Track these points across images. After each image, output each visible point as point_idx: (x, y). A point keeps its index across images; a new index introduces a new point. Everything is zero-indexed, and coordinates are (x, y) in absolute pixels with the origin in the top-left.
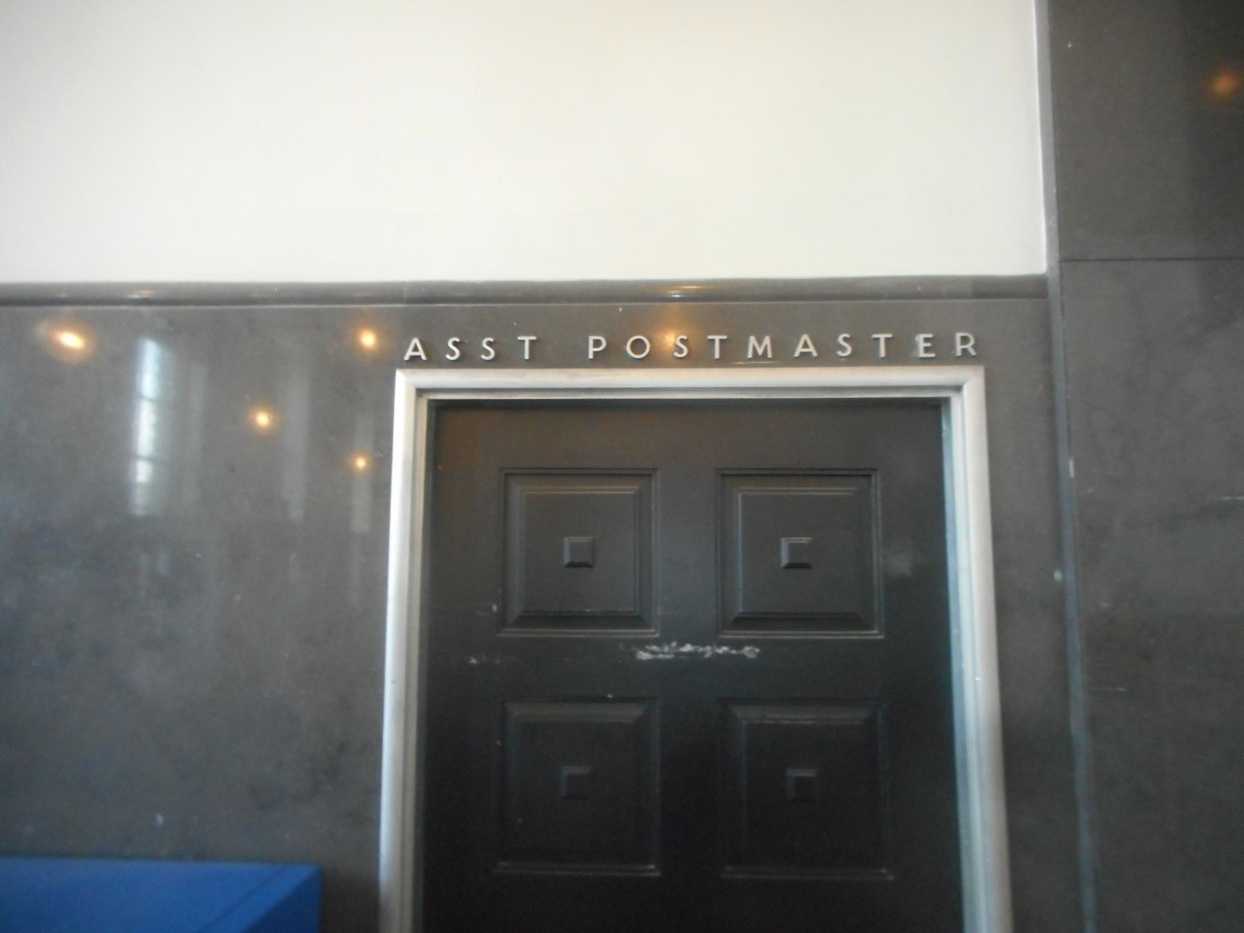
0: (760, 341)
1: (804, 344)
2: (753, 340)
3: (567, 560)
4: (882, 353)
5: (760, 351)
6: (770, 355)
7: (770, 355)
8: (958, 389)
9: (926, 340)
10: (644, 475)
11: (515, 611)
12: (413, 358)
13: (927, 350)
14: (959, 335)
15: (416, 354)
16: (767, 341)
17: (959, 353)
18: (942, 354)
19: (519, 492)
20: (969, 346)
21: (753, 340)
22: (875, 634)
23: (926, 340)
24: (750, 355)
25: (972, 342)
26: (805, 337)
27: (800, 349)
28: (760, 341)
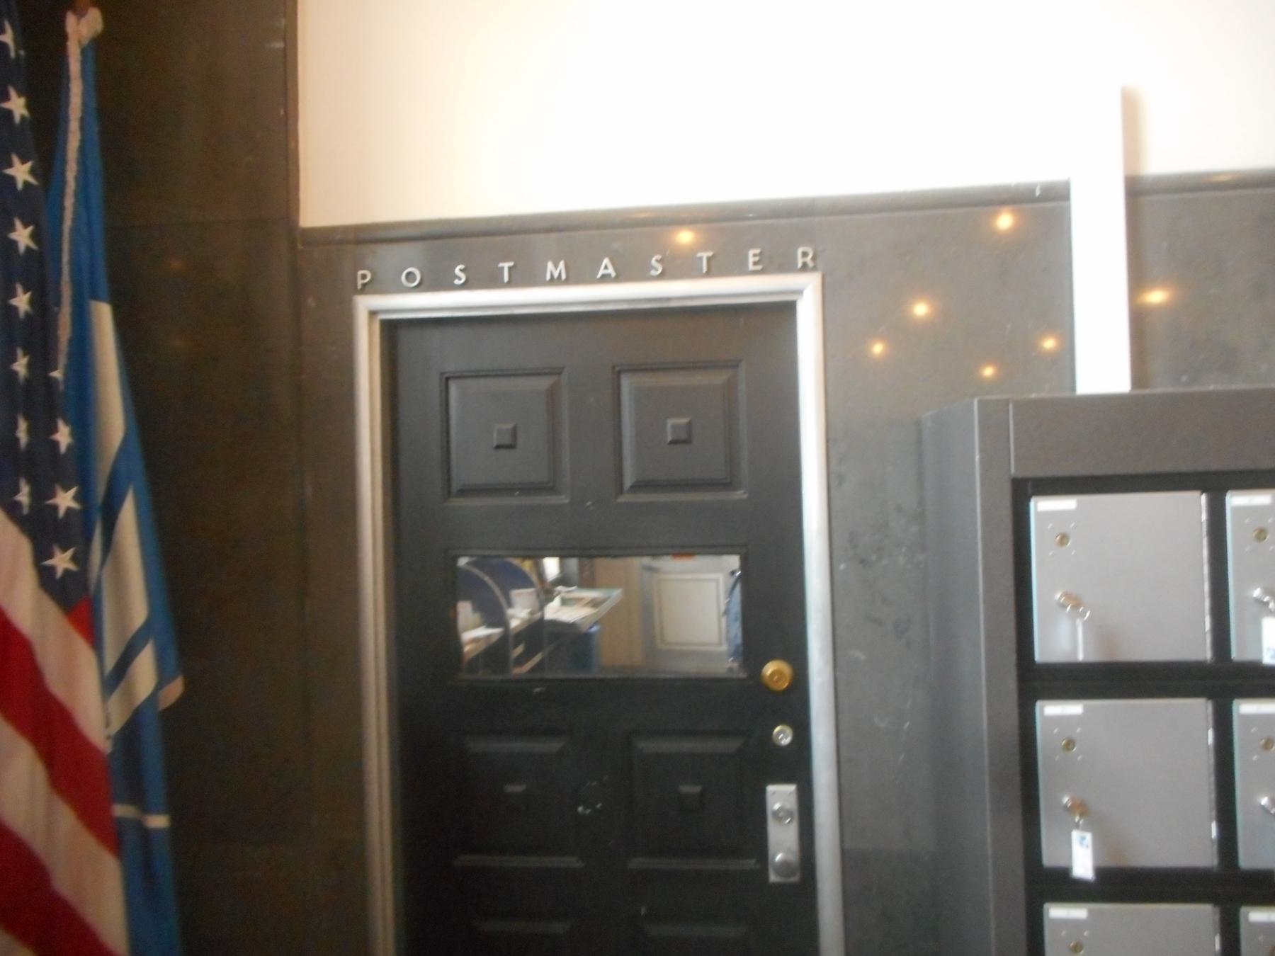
0: (556, 266)
1: (606, 267)
2: (550, 265)
3: (669, 439)
4: (506, 279)
5: (556, 275)
6: (564, 276)
7: (564, 276)
8: (800, 292)
9: (755, 255)
10: (557, 372)
11: (628, 481)
12: (603, 276)
13: (755, 263)
14: (800, 251)
15: (606, 272)
16: (562, 265)
17: (800, 265)
18: (786, 266)
19: (627, 383)
20: (808, 259)
21: (550, 265)
22: (564, 499)
23: (755, 255)
24: (548, 277)
25: (811, 256)
26: (606, 261)
27: (602, 272)
28: (556, 266)
